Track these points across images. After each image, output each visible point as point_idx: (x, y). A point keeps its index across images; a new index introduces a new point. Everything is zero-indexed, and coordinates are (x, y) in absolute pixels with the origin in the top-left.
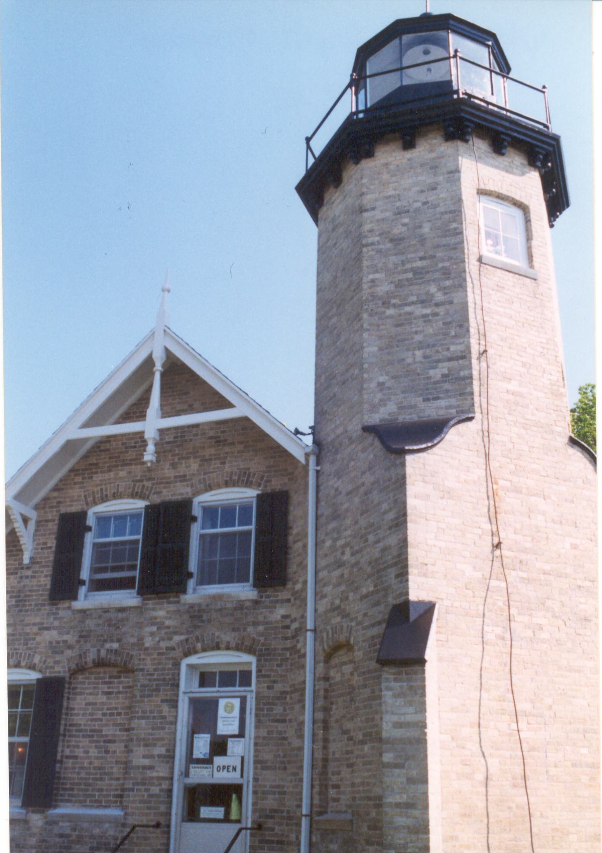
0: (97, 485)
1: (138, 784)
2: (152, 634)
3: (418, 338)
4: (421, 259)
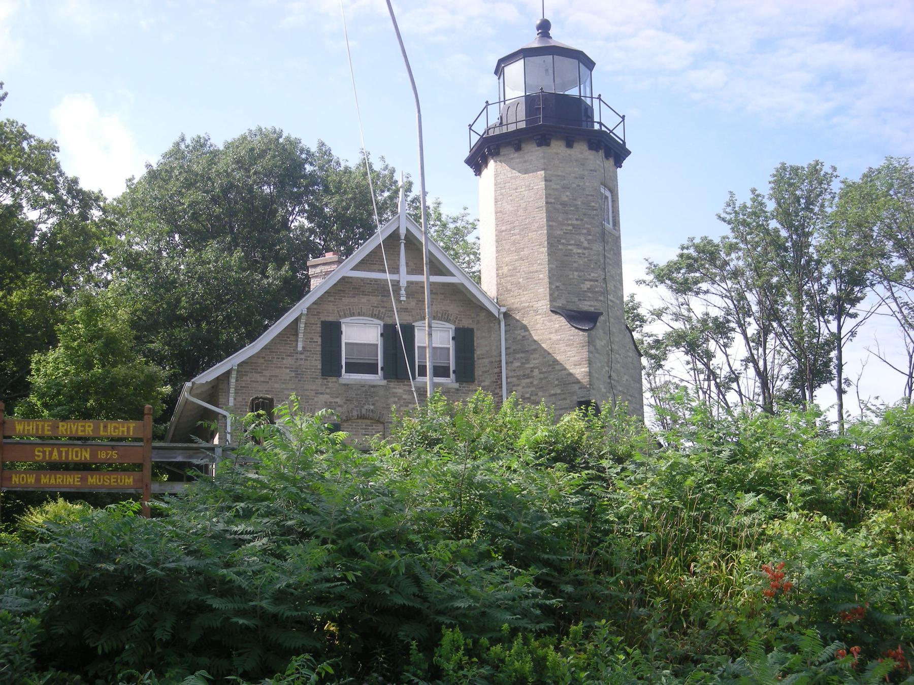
0: (346, 305)
3: (575, 265)
4: (577, 220)
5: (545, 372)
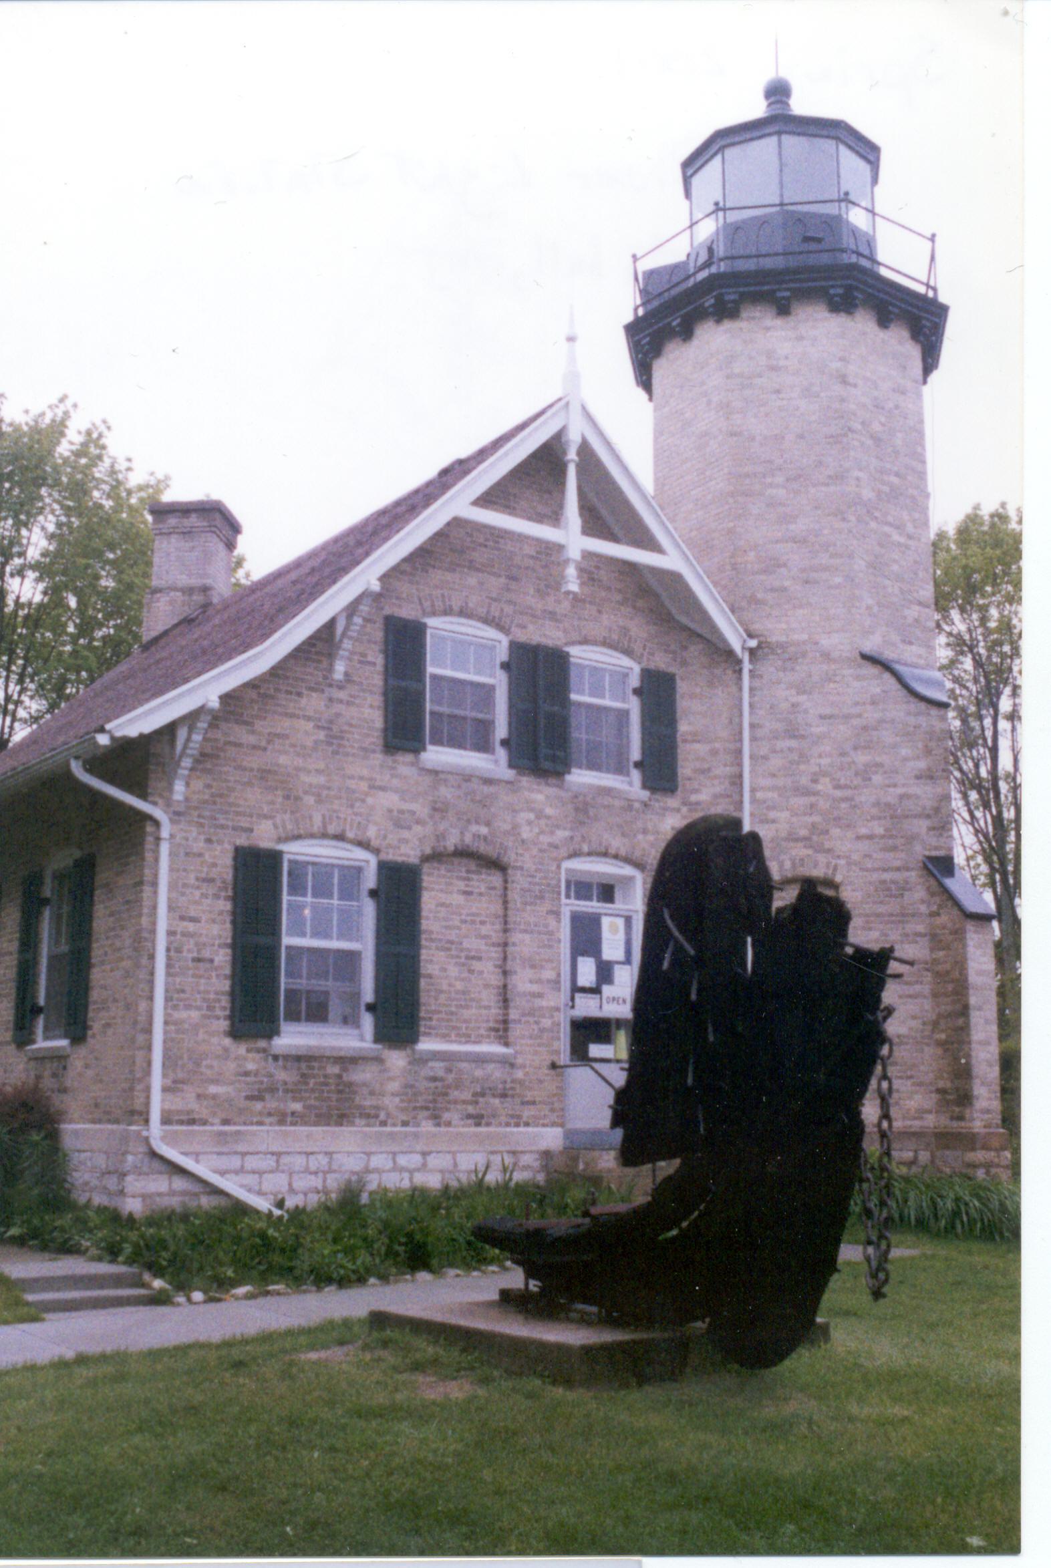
1: (524, 1015)
2: (529, 823)
5: (846, 787)
